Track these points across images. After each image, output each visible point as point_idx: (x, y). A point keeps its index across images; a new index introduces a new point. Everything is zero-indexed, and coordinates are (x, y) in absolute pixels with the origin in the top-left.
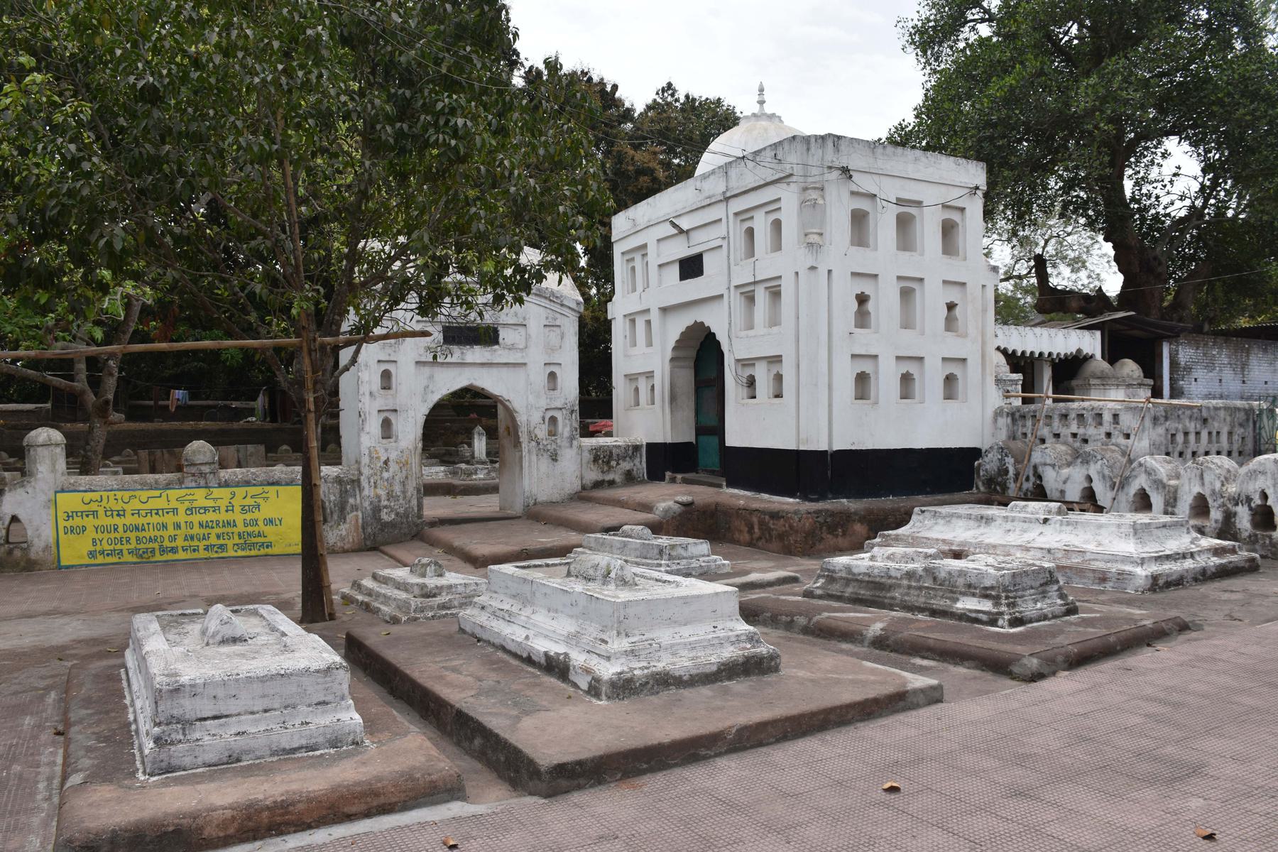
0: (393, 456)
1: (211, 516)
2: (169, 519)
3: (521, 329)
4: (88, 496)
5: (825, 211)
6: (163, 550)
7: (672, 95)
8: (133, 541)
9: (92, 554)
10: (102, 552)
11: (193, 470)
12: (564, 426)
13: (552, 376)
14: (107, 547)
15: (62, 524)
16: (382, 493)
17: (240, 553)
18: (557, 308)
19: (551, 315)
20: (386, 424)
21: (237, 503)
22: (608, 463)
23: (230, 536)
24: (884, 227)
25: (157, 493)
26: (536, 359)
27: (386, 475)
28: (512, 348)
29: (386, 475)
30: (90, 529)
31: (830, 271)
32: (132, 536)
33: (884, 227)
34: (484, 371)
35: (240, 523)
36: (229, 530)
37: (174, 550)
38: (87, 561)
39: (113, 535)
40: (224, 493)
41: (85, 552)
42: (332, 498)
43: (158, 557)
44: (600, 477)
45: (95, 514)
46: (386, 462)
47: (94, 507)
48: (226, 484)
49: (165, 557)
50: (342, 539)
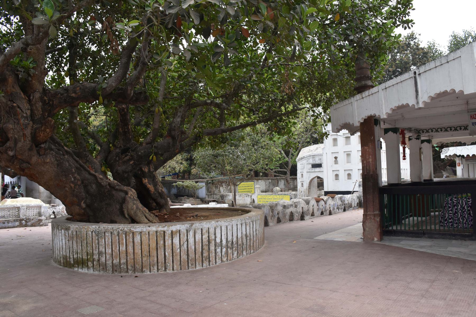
20: (302, 184)
40: (278, 196)
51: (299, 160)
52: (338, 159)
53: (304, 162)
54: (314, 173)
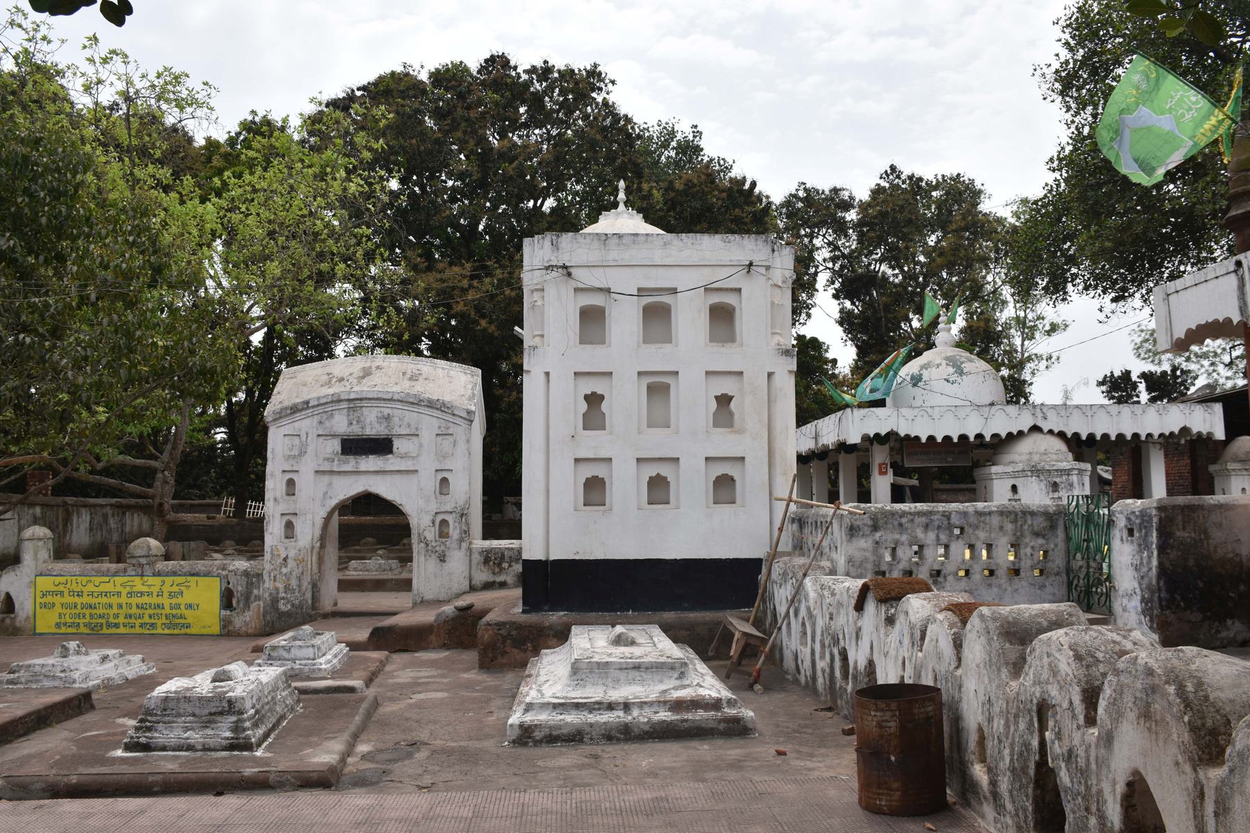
0: (292, 553)
1: (145, 599)
2: (114, 600)
3: (414, 439)
4: (58, 579)
5: (542, 314)
6: (109, 625)
7: (898, 177)
8: (87, 616)
9: (58, 625)
10: (65, 624)
11: (134, 561)
12: (455, 528)
13: (444, 481)
14: (68, 620)
15: (39, 600)
16: (280, 586)
17: (167, 631)
18: (450, 418)
19: (443, 424)
20: (289, 526)
21: (166, 589)
22: (499, 564)
23: (159, 616)
24: (625, 321)
25: (106, 579)
26: (427, 467)
27: (284, 570)
28: (404, 456)
29: (284, 570)
30: (58, 605)
31: (547, 374)
32: (87, 612)
33: (625, 321)
34: (378, 478)
35: (167, 606)
36: (159, 611)
37: (116, 626)
38: (53, 630)
39: (73, 611)
40: (157, 581)
41: (53, 624)
42: (240, 588)
43: (105, 631)
44: (491, 578)
45: (62, 593)
46: (285, 559)
47: (61, 588)
48: (159, 574)
49: (110, 631)
50: (247, 624)
51: (280, 415)
52: (604, 406)
53: (306, 424)
54: (353, 478)
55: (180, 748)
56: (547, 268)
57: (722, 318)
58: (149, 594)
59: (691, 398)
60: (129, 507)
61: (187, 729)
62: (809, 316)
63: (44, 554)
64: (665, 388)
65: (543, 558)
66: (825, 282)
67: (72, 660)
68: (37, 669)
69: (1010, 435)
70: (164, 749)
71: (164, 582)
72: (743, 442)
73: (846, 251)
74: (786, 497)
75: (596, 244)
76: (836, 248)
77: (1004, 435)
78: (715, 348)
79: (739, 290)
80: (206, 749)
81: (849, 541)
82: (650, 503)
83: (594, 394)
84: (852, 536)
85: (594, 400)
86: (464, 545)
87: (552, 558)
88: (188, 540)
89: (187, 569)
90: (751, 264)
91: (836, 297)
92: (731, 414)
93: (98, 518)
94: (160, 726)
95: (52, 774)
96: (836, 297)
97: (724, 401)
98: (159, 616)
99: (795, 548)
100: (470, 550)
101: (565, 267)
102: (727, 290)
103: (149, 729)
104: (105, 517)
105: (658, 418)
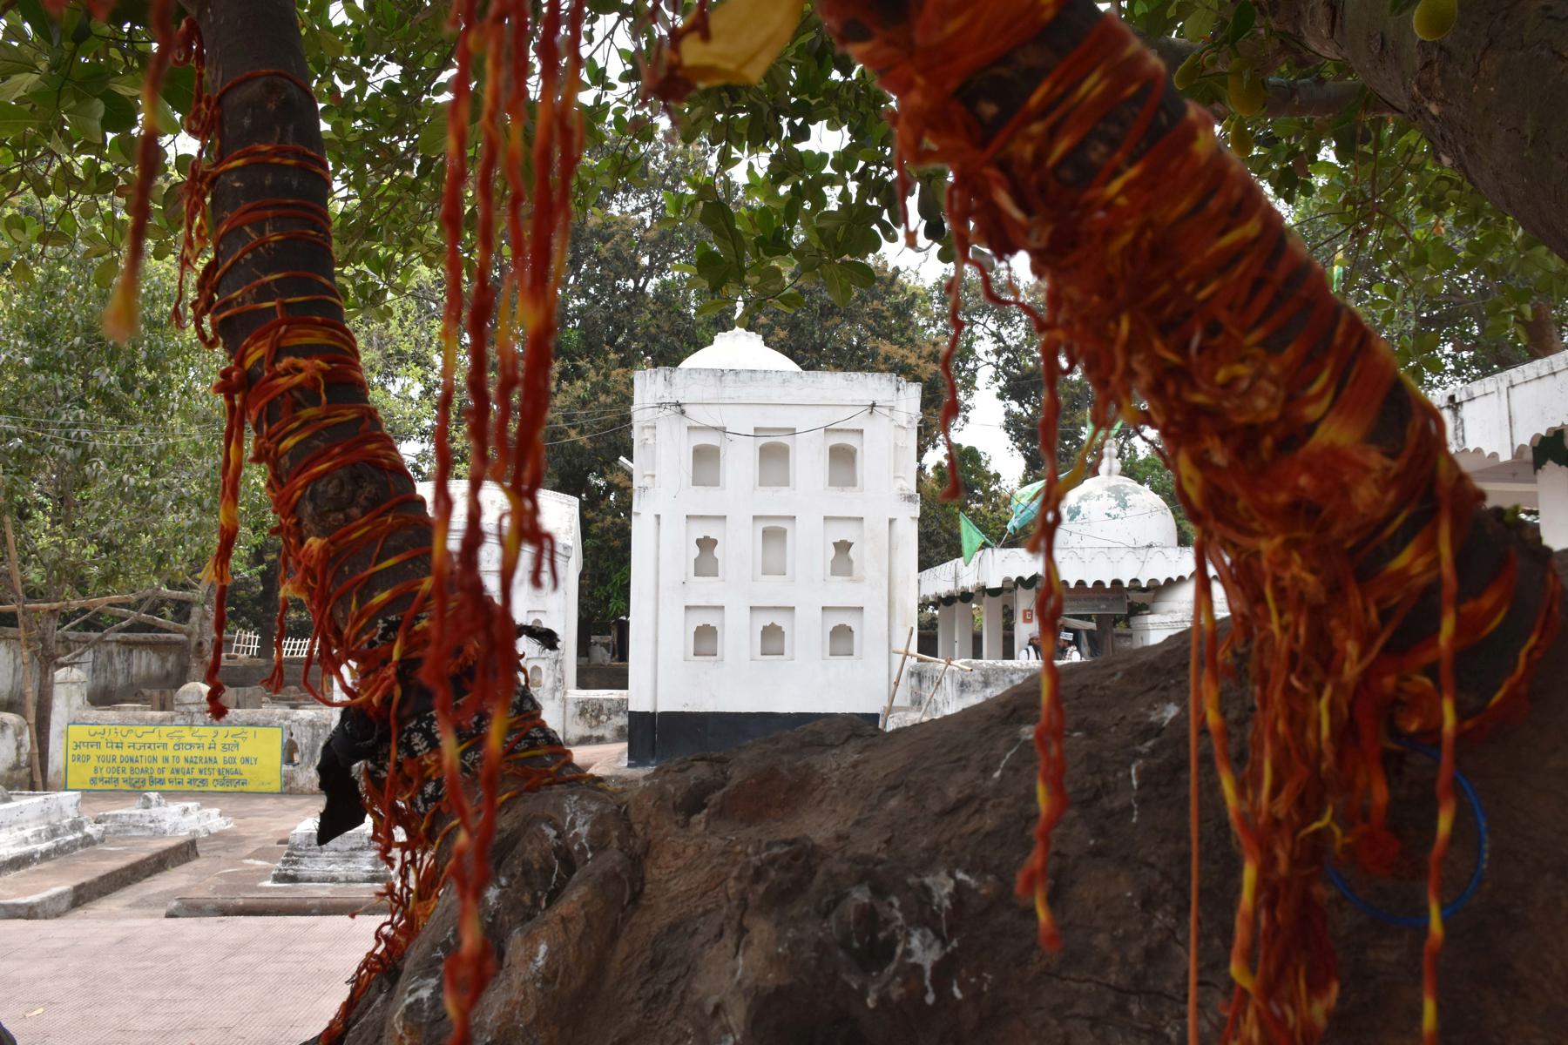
1: (195, 752)
2: (159, 753)
9: (93, 781)
11: (183, 709)
14: (105, 775)
15: (71, 752)
17: (219, 788)
21: (219, 741)
22: (597, 717)
23: (211, 771)
24: (740, 461)
25: (150, 729)
31: (658, 517)
32: (128, 766)
33: (740, 461)
35: (220, 761)
36: (210, 766)
44: (587, 732)
45: (98, 744)
47: (97, 738)
52: (717, 552)
55: (324, 880)
56: (660, 405)
57: (843, 458)
58: (200, 746)
59: (809, 545)
60: (136, 644)
61: (330, 863)
62: (966, 420)
63: (78, 699)
64: (782, 533)
65: (651, 710)
66: (987, 379)
67: (155, 811)
68: (125, 819)
69: (1169, 581)
70: (309, 880)
71: (217, 733)
72: (865, 592)
73: (1013, 343)
74: (903, 649)
75: (711, 380)
76: (1000, 338)
77: (1162, 582)
78: (835, 492)
79: (861, 432)
80: (349, 881)
81: (960, 696)
82: (763, 654)
83: (706, 538)
84: (962, 691)
85: (706, 544)
86: (558, 695)
87: (660, 709)
88: (243, 685)
89: (244, 718)
90: (873, 405)
91: (1001, 397)
92: (850, 561)
93: (102, 657)
94: (306, 860)
95: (220, 898)
96: (1001, 397)
97: (843, 547)
98: (211, 771)
99: (913, 703)
100: (564, 700)
101: (678, 404)
102: (848, 431)
103: (295, 863)
104: (110, 655)
105: (773, 568)
